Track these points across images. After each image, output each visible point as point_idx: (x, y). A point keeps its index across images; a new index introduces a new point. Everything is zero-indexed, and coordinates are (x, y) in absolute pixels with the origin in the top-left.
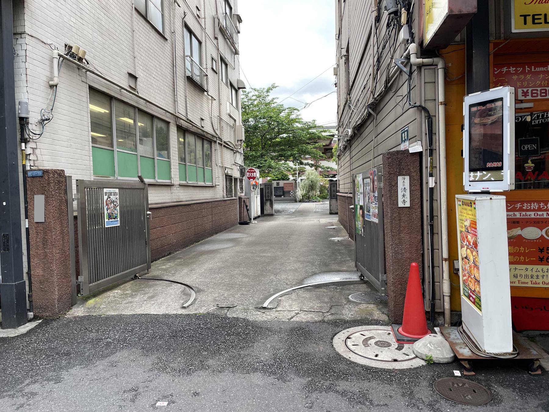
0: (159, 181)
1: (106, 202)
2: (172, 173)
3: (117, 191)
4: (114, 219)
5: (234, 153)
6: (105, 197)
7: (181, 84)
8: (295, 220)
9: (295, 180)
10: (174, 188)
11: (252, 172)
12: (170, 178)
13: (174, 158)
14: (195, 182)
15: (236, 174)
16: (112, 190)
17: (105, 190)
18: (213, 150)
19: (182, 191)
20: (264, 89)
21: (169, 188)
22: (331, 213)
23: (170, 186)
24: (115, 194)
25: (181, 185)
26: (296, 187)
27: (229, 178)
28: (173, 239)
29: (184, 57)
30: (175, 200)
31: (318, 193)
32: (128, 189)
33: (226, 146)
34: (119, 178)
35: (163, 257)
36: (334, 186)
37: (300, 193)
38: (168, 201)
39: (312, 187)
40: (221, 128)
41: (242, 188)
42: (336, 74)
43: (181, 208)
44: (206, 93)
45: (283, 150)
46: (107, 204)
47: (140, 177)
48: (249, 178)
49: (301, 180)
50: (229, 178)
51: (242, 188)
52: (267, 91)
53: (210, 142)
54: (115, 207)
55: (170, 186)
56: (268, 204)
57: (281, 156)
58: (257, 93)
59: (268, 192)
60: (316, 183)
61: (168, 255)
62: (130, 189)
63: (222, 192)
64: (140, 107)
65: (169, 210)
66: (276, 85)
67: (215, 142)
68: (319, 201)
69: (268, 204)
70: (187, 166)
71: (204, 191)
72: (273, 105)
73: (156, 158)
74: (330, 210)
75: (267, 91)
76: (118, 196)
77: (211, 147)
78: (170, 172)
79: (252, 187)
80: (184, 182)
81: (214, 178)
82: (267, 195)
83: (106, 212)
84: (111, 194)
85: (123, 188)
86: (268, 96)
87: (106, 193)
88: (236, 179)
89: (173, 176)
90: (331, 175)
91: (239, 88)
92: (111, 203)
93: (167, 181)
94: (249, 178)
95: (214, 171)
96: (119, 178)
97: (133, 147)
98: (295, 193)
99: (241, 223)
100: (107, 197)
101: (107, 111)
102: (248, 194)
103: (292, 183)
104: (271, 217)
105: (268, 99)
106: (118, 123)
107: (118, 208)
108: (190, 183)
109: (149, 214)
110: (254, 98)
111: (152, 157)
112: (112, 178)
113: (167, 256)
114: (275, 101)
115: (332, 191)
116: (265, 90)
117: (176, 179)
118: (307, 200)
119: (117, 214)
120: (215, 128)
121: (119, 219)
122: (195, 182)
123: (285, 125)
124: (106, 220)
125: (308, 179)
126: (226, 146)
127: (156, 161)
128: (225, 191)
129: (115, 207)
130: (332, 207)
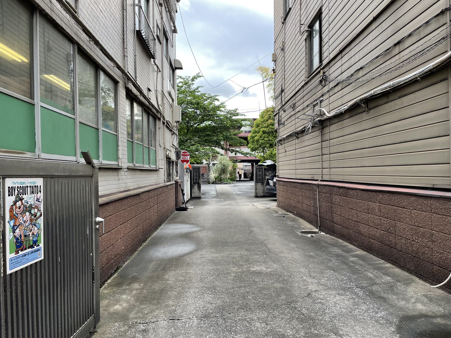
0: (105, 162)
1: (11, 210)
2: (120, 152)
3: (39, 182)
4: (32, 247)
5: (172, 134)
6: (9, 200)
7: (131, 39)
8: (228, 205)
9: (208, 164)
10: (122, 173)
11: (185, 155)
12: (117, 159)
13: (123, 131)
14: (142, 165)
15: (173, 157)
16: (28, 182)
17: (9, 182)
18: (157, 128)
19: (129, 177)
20: (189, 77)
21: (115, 173)
22: (257, 197)
23: (117, 169)
24: (34, 189)
25: (129, 169)
26: (209, 170)
27: (168, 159)
28: (121, 246)
29: (134, 5)
30: (122, 189)
31: (228, 176)
32: (63, 177)
33: (168, 126)
34: (44, 156)
35: (109, 278)
36: (260, 171)
37: (213, 176)
38: (114, 191)
39: (223, 170)
40: (163, 104)
41: (177, 172)
42: (275, 61)
43: (130, 200)
44: (152, 60)
45: (209, 135)
46: (13, 217)
47: (85, 155)
48: (183, 161)
49: (214, 164)
50: (168, 159)
51: (177, 172)
52: (193, 80)
53: (156, 118)
54: (33, 222)
55: (117, 169)
56: (196, 187)
57: (206, 141)
58: (182, 80)
59: (196, 176)
60: (227, 167)
61: (116, 271)
62: (66, 177)
63: (164, 177)
64: (81, 43)
65: (118, 204)
66: (201, 75)
67: (159, 119)
68: (230, 183)
69: (196, 187)
70: (135, 145)
71: (150, 176)
72: (196, 93)
73: (101, 128)
74: (256, 193)
75: (193, 80)
76: (41, 195)
77: (155, 125)
78: (117, 150)
79: (185, 171)
80: (131, 165)
81: (157, 160)
82: (195, 178)
83: (9, 236)
84: (24, 190)
85: (52, 177)
86: (193, 84)
87: (11, 190)
88: (173, 162)
89: (120, 156)
90: (239, 161)
91: (177, 68)
92: (23, 213)
93: (113, 163)
94: (183, 161)
95: (157, 153)
96: (44, 156)
97: (70, 106)
98: (208, 176)
99: (178, 209)
100: (13, 198)
101: (26, 60)
102: (182, 177)
103: (206, 167)
104: (198, 201)
105: (193, 87)
106: (44, 82)
107: (41, 221)
108: (138, 165)
109: (99, 223)
110: (180, 85)
111: (94, 126)
112: (29, 155)
113: (114, 273)
114: (200, 89)
115: (258, 175)
116: (191, 79)
117: (124, 163)
118: (219, 182)
119: (38, 235)
120: (160, 104)
121: (42, 245)
122: (142, 165)
123: (209, 113)
124: (9, 256)
125: (221, 163)
126: (168, 126)
127: (101, 133)
128: (166, 175)
129: (33, 222)
130: (257, 191)
